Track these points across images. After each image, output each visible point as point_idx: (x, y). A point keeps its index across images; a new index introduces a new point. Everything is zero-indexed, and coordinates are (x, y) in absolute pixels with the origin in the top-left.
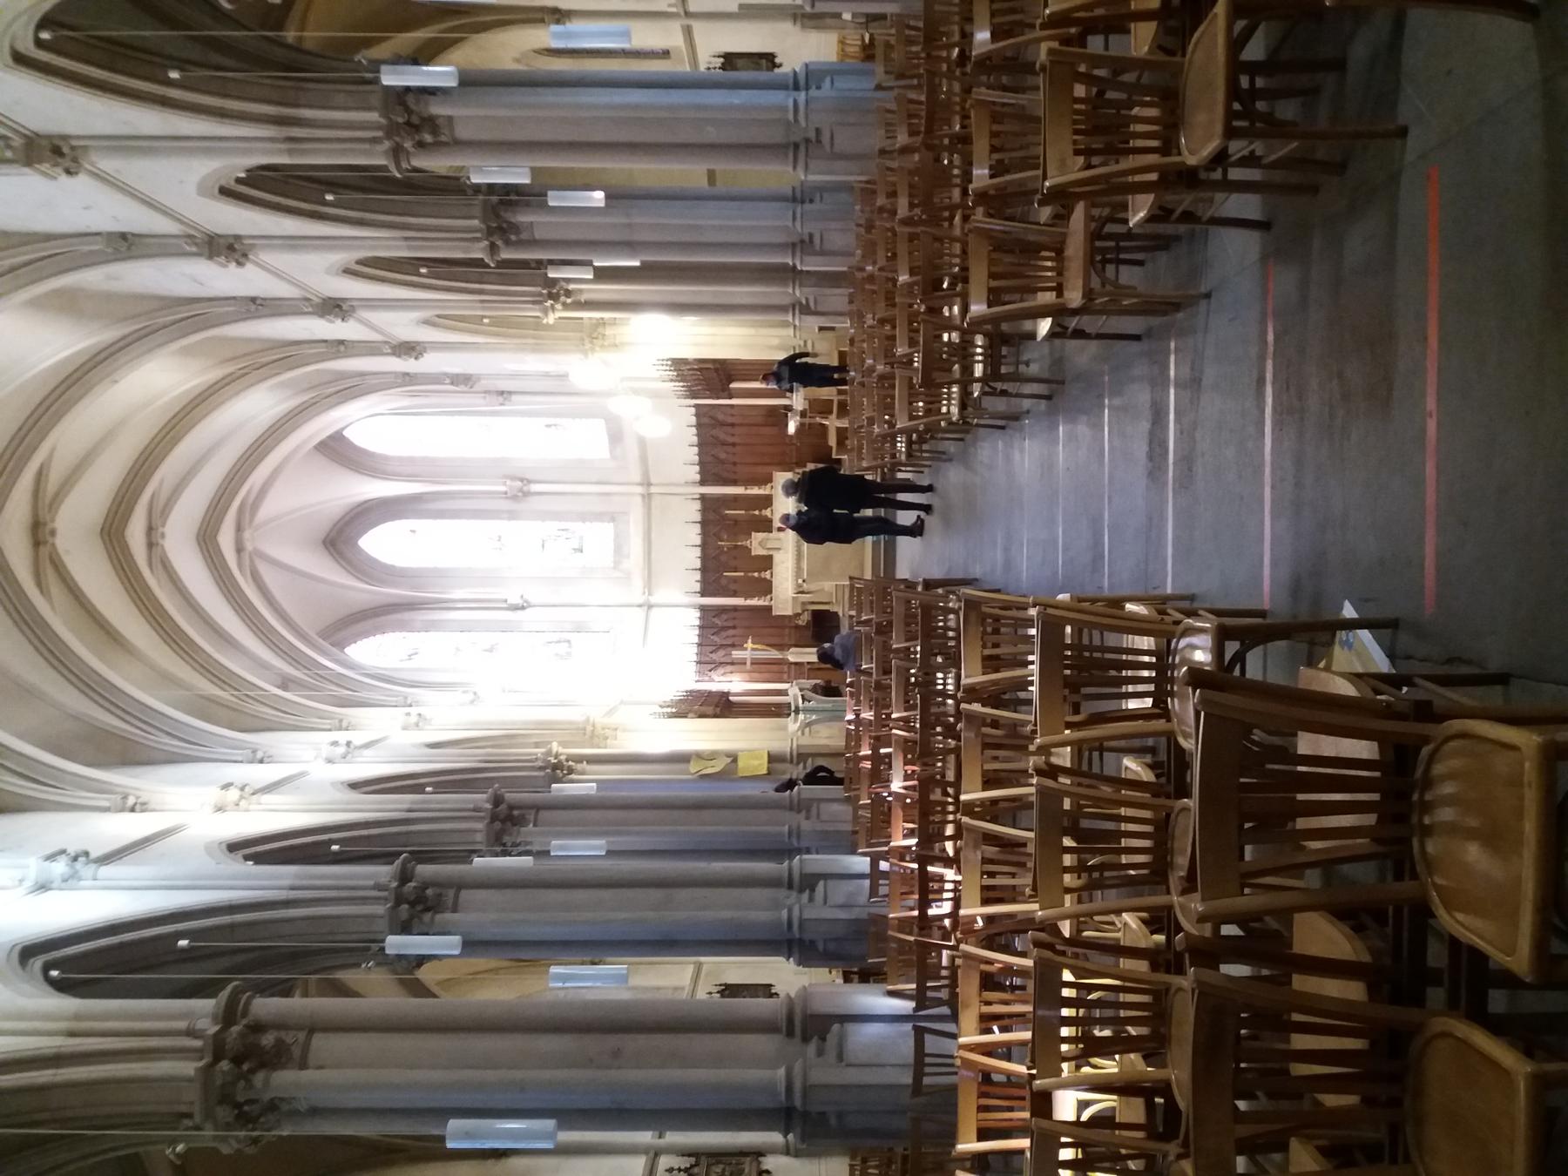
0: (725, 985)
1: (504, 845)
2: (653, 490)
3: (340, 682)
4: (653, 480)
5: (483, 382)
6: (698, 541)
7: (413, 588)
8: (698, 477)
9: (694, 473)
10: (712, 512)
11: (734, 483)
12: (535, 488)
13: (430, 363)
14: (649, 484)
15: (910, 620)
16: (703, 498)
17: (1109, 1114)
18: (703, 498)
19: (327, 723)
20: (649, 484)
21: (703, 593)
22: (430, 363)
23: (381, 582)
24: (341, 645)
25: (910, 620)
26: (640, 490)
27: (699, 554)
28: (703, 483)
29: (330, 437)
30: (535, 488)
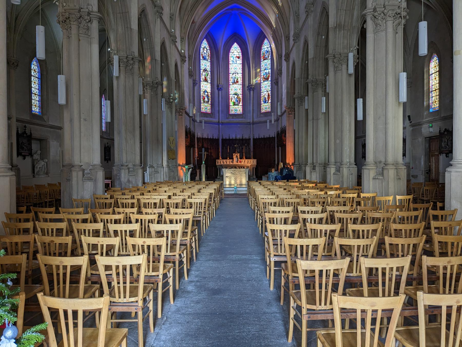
0: (110, 147)
1: (146, 86)
2: (252, 125)
3: (195, 39)
4: (254, 125)
5: (280, 78)
6: (238, 138)
7: (223, 58)
8: (255, 138)
9: (256, 136)
10: (247, 141)
11: (254, 148)
12: (252, 92)
13: (284, 64)
14: (253, 124)
15: (190, 197)
16: (249, 139)
17: (368, 271)
18: (249, 139)
19: (182, 35)
20: (253, 124)
21: (222, 140)
22: (284, 64)
23: (224, 49)
24: (206, 38)
25: (190, 197)
26: (251, 121)
27: (234, 138)
28: (254, 139)
29: (265, 35)
30: (252, 92)
